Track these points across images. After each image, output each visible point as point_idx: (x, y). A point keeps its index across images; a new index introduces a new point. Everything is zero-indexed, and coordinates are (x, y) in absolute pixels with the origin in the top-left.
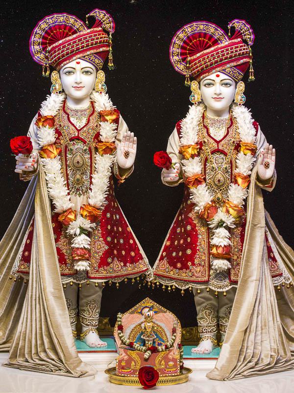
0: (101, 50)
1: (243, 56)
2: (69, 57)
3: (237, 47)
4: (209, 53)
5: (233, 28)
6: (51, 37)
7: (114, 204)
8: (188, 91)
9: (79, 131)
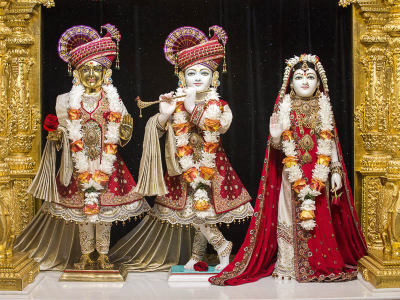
0: (217, 57)
1: (217, 53)
2: (191, 62)
3: (214, 47)
4: (190, 51)
5: (212, 32)
6: (181, 45)
7: (229, 168)
8: (177, 79)
9: (90, 114)
